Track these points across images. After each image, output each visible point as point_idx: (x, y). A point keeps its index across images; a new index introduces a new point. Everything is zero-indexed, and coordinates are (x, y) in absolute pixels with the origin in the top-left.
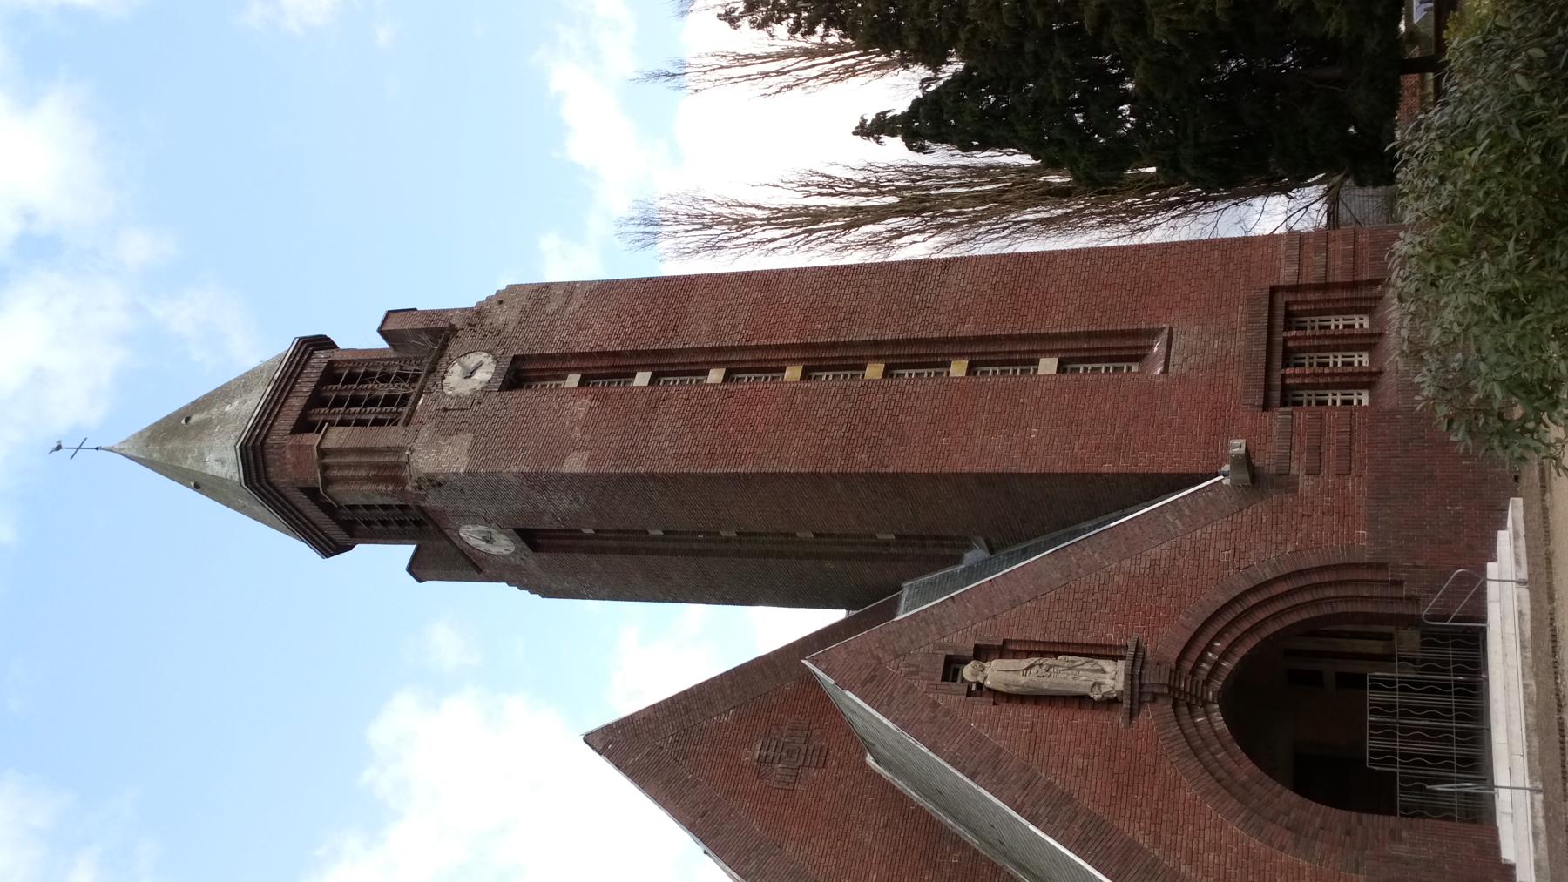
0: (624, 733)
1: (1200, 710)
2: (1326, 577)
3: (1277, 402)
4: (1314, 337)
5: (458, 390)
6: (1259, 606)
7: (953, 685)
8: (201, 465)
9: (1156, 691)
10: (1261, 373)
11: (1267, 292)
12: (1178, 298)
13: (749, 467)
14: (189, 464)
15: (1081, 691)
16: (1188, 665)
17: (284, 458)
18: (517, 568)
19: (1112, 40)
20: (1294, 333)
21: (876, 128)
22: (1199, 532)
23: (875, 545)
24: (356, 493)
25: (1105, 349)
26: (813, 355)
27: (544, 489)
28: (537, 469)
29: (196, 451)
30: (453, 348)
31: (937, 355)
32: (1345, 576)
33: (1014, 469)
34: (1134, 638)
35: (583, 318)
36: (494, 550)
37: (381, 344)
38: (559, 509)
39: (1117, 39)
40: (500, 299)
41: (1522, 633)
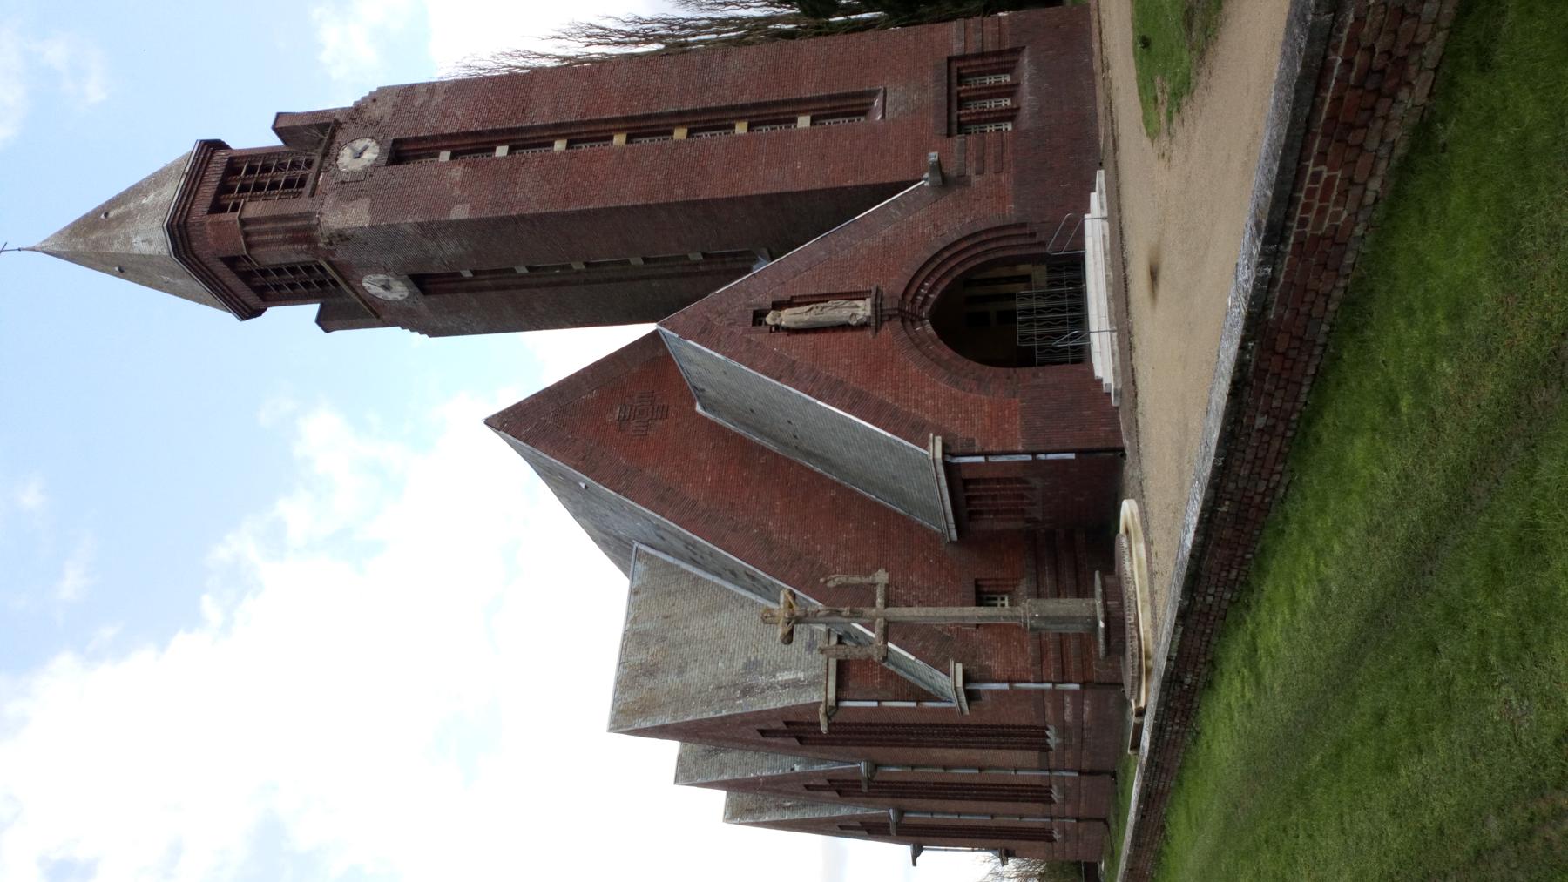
0: (515, 415)
1: (918, 323)
3: (956, 132)
4: (976, 89)
5: (351, 168)
6: (950, 258)
7: (761, 328)
8: (129, 247)
9: (891, 313)
10: (945, 113)
11: (946, 60)
12: (888, 68)
13: (596, 204)
14: (116, 248)
15: (844, 320)
16: (909, 298)
17: (206, 233)
20: (964, 87)
22: (911, 217)
23: (689, 265)
24: (275, 254)
25: (843, 107)
26: (633, 125)
27: (434, 237)
29: (122, 236)
30: (340, 137)
31: (725, 119)
32: (1002, 234)
33: (787, 189)
34: (875, 285)
35: (446, 109)
36: (391, 296)
37: (275, 141)
38: (445, 253)
40: (374, 98)
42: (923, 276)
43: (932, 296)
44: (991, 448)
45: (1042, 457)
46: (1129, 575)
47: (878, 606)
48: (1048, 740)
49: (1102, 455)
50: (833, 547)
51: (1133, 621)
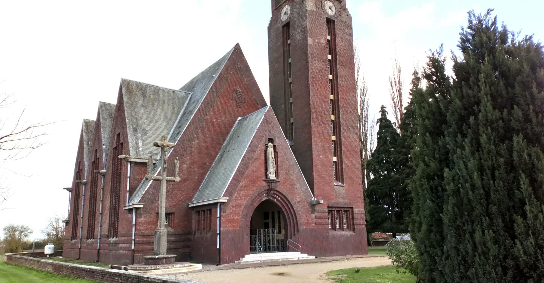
0: (240, 54)
2: (295, 220)
4: (342, 216)
6: (288, 206)
7: (267, 141)
10: (335, 206)
11: (352, 207)
13: (311, 88)
16: (275, 192)
18: (277, 21)
19: (405, 170)
20: (343, 212)
21: (383, 112)
27: (302, 32)
28: (308, 30)
31: (337, 133)
33: (313, 153)
36: (282, 15)
38: (296, 35)
39: (405, 171)
40: (348, 15)
41: (289, 258)
42: (282, 197)
43: (276, 200)
44: (222, 219)
45: (218, 237)
46: (175, 266)
47: (167, 177)
48: (112, 238)
49: (218, 257)
50: (188, 163)
51: (158, 267)
